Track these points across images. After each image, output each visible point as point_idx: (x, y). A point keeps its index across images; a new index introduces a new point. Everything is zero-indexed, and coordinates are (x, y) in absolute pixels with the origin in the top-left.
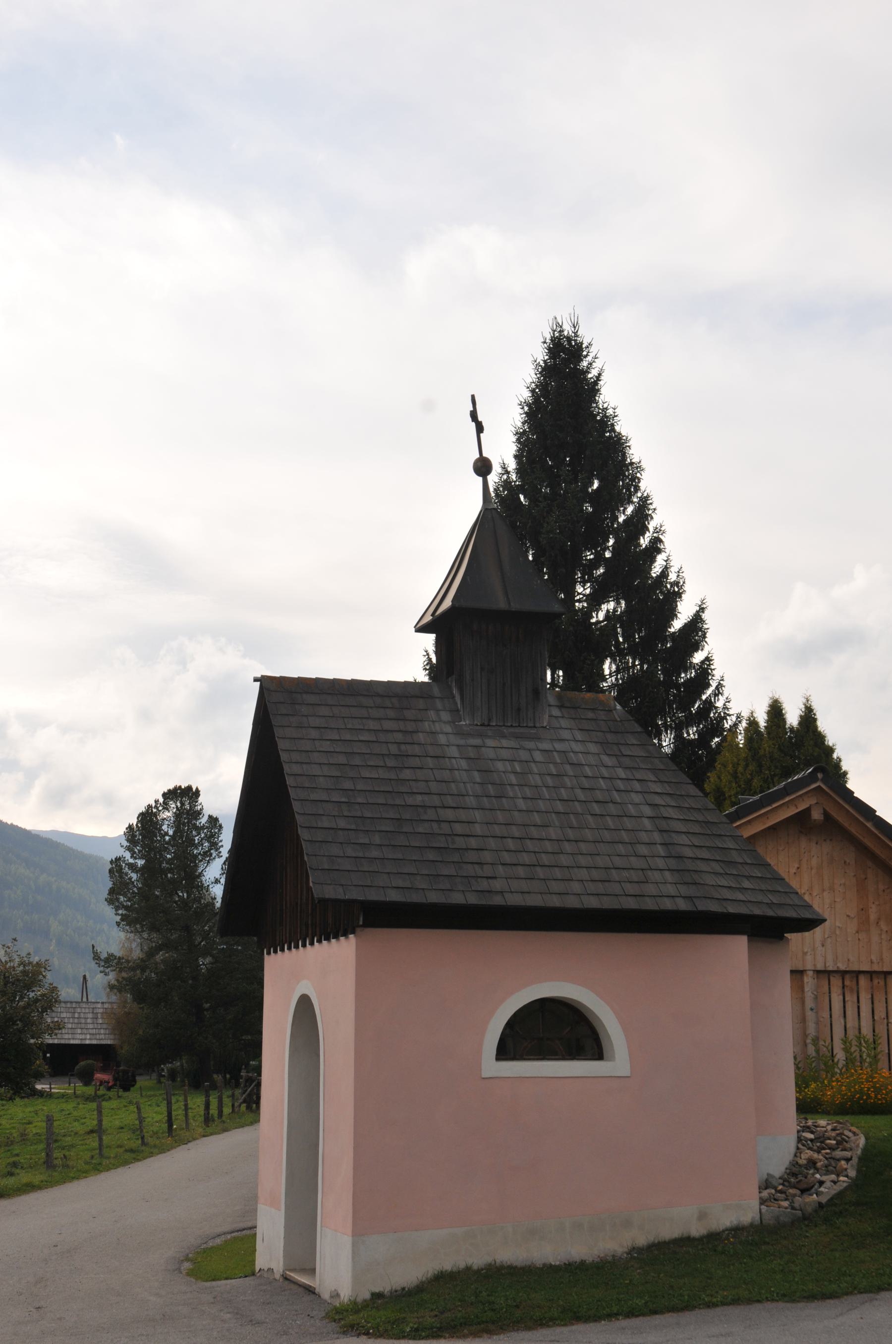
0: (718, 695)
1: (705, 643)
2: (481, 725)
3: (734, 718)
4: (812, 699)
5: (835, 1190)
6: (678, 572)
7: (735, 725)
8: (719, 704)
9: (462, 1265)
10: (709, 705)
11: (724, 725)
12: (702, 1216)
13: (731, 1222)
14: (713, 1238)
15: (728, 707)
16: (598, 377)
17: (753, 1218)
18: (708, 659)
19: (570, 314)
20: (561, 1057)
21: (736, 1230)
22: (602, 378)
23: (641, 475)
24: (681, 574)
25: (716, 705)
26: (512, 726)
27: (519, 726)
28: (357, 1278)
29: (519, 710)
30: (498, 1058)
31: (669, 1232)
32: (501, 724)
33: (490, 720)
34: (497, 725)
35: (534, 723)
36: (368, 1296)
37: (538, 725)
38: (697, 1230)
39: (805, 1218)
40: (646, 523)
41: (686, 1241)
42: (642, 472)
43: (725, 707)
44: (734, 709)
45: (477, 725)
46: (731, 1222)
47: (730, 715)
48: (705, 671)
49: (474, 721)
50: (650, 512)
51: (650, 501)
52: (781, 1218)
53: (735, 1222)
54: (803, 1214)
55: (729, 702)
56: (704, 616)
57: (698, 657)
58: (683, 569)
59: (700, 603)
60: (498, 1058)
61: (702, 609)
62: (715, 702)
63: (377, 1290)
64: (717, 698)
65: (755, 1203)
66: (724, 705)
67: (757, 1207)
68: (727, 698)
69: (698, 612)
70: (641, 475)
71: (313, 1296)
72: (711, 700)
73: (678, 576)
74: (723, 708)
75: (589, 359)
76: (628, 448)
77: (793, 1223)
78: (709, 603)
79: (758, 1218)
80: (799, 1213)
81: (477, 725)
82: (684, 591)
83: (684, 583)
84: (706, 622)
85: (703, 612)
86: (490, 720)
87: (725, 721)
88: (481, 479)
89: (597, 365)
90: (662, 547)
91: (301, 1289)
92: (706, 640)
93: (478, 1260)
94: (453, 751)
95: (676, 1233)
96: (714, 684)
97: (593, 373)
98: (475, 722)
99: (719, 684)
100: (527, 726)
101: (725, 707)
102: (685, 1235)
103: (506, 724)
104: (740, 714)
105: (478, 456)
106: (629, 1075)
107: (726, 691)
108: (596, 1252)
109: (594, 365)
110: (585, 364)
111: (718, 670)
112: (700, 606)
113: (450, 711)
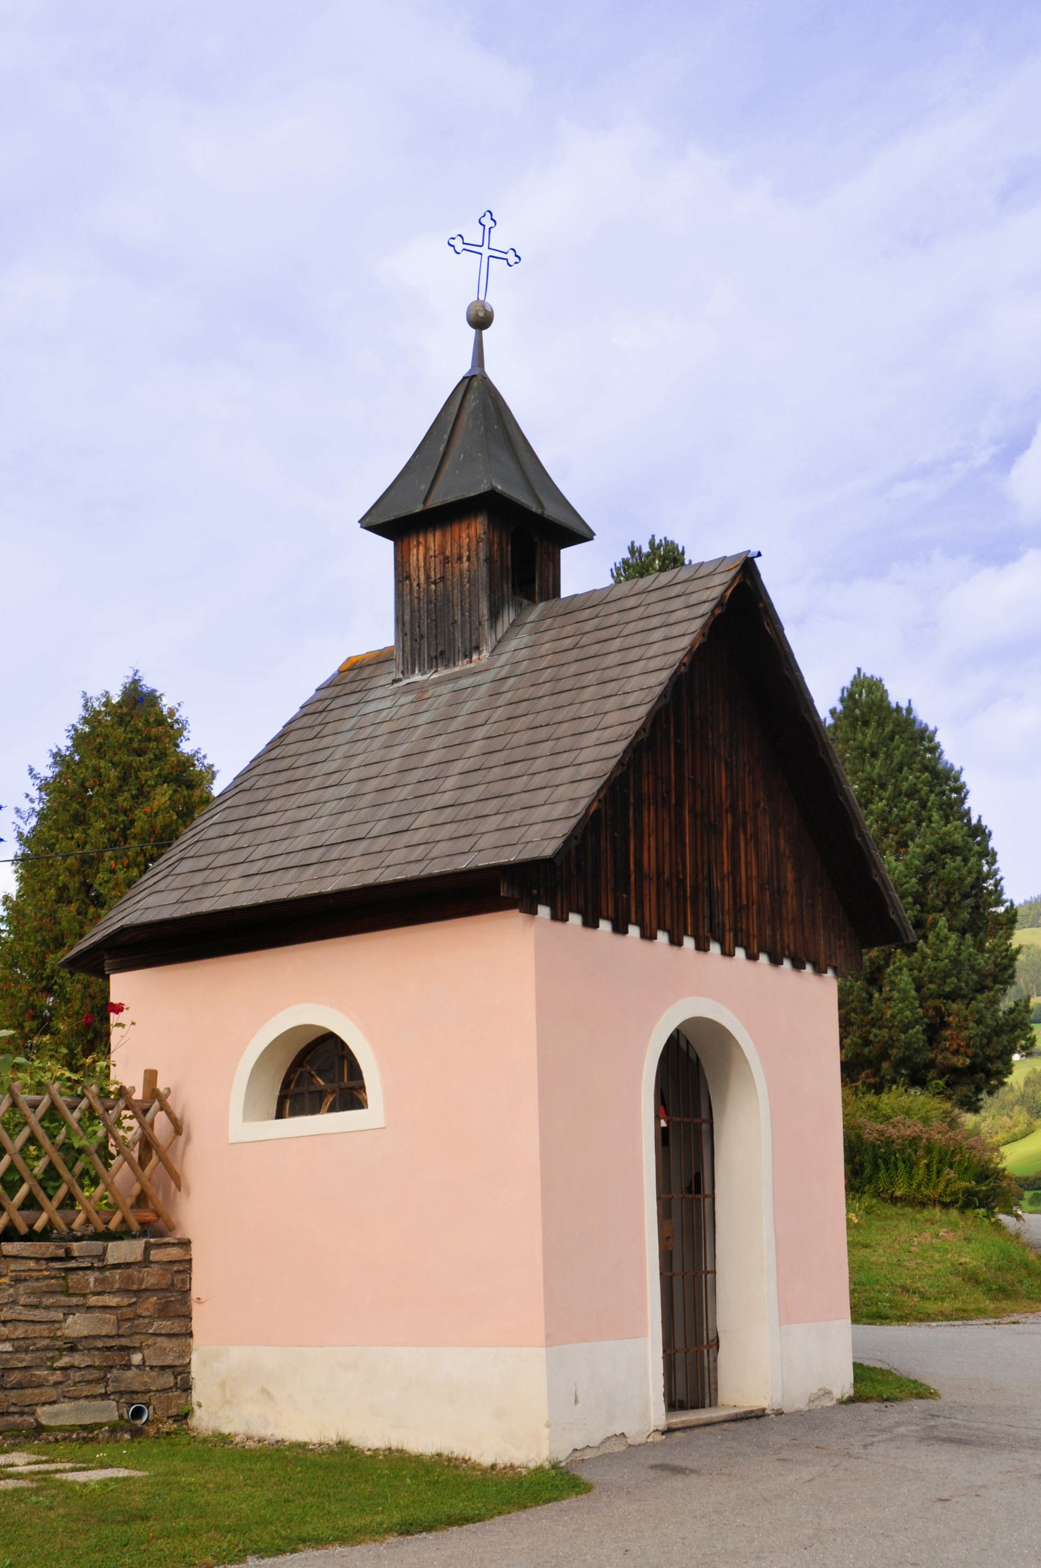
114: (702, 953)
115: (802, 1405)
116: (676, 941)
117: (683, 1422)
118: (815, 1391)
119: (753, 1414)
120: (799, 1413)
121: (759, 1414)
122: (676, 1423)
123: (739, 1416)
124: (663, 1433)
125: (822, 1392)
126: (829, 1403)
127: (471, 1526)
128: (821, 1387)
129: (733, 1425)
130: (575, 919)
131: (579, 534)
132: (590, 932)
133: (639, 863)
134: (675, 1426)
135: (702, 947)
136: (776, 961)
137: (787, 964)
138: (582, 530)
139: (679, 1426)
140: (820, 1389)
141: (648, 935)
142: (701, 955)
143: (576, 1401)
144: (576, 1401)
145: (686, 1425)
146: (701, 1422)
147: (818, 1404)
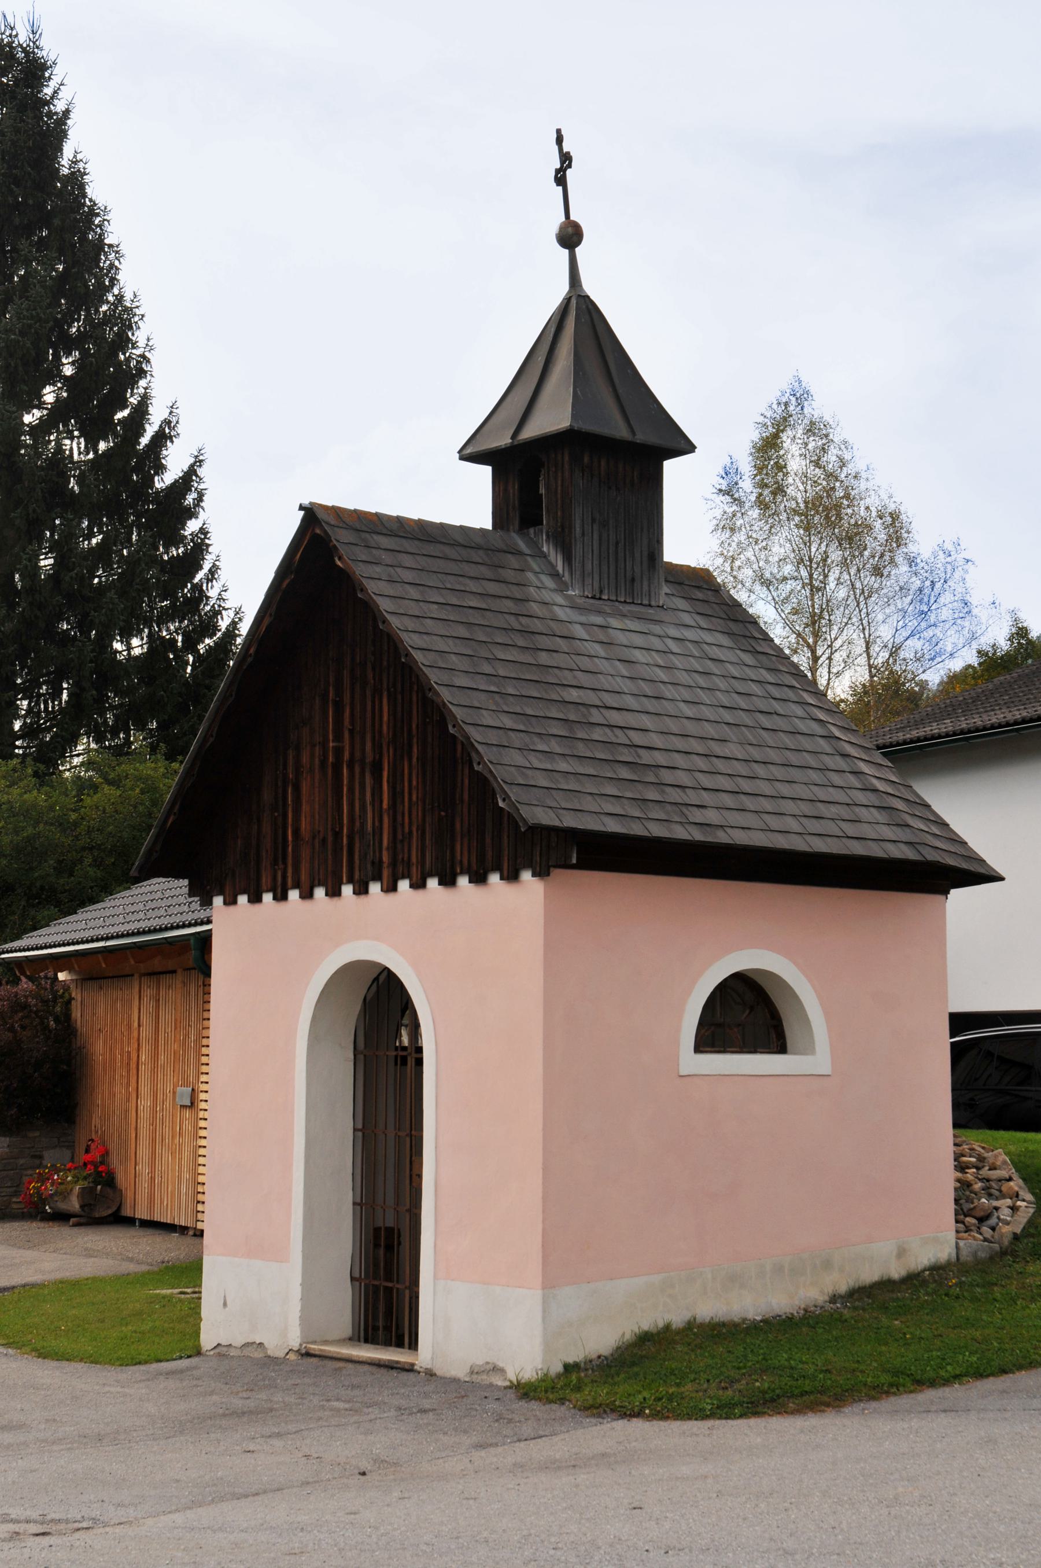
0: (212, 582)
1: (201, 510)
2: (592, 598)
3: (231, 613)
4: (1022, 616)
5: (1024, 1217)
6: (172, 407)
7: (234, 624)
8: (213, 593)
9: (661, 1324)
10: (199, 595)
11: (217, 622)
12: (901, 1252)
13: (929, 1259)
14: (913, 1280)
15: (224, 597)
16: (67, 113)
17: (950, 1254)
18: (203, 531)
19: (28, 13)
20: (738, 1050)
21: (936, 1269)
22: (72, 115)
23: (120, 263)
24: (174, 410)
25: (208, 595)
26: (625, 602)
27: (633, 603)
28: (548, 1347)
29: (633, 580)
30: (698, 1048)
31: (869, 1275)
32: (614, 598)
33: (601, 592)
34: (609, 599)
35: (650, 600)
36: (559, 1368)
37: (653, 603)
38: (896, 1272)
39: (1003, 1253)
40: (130, 334)
41: (886, 1285)
42: (121, 259)
43: (220, 598)
44: (232, 601)
45: (588, 597)
46: (929, 1259)
47: (226, 609)
48: (199, 547)
49: (584, 591)
50: (136, 319)
51: (137, 304)
52: (979, 1253)
53: (933, 1260)
54: (1001, 1248)
55: (225, 591)
56: (201, 472)
57: (192, 526)
58: (178, 404)
59: (196, 454)
60: (698, 1048)
61: (198, 462)
62: (207, 589)
63: (571, 1360)
64: (210, 584)
65: (951, 1236)
66: (220, 595)
67: (953, 1241)
68: (223, 586)
69: (192, 466)
70: (120, 263)
71: (411, 1375)
72: (202, 586)
73: (171, 413)
74: (218, 599)
75: (53, 84)
76: (106, 222)
77: (991, 1258)
78: (207, 456)
79: (954, 1255)
80: (996, 1246)
81: (588, 597)
82: (178, 434)
83: (177, 422)
84: (204, 480)
85: (200, 466)
86: (601, 592)
87: (219, 617)
88: (567, 251)
89: (65, 94)
90: (149, 369)
91: (366, 1368)
92: (202, 504)
93: (677, 1318)
94: (580, 632)
95: (876, 1278)
96: (207, 566)
97: (59, 106)
98: (586, 593)
99: (214, 565)
100: (641, 604)
101: (220, 598)
102: (885, 1278)
103: (619, 599)
104: (240, 609)
105: (563, 219)
106: (830, 1073)
107: (223, 575)
108: (797, 1303)
109: (61, 95)
110: (48, 91)
111: (218, 546)
112: (196, 457)
113: (550, 575)
114: (336, 899)
115: (460, 1372)
116: (334, 892)
117: (321, 1350)
118: (480, 1362)
119: (399, 1366)
120: (455, 1380)
121: (407, 1367)
122: (314, 1349)
123: (382, 1363)
124: (302, 1355)
125: (490, 1367)
126: (500, 1382)
127: (65, 1363)
128: (488, 1360)
129: (374, 1369)
130: (243, 899)
131: (683, 446)
132: (257, 907)
133: (296, 832)
134: (313, 1352)
135: (362, 890)
136: (448, 881)
137: (463, 881)
138: (683, 445)
139: (317, 1353)
140: (488, 1363)
141: (307, 895)
142: (363, 899)
143: (225, 1305)
144: (225, 1305)
145: (324, 1354)
146: (339, 1356)
147: (485, 1379)
